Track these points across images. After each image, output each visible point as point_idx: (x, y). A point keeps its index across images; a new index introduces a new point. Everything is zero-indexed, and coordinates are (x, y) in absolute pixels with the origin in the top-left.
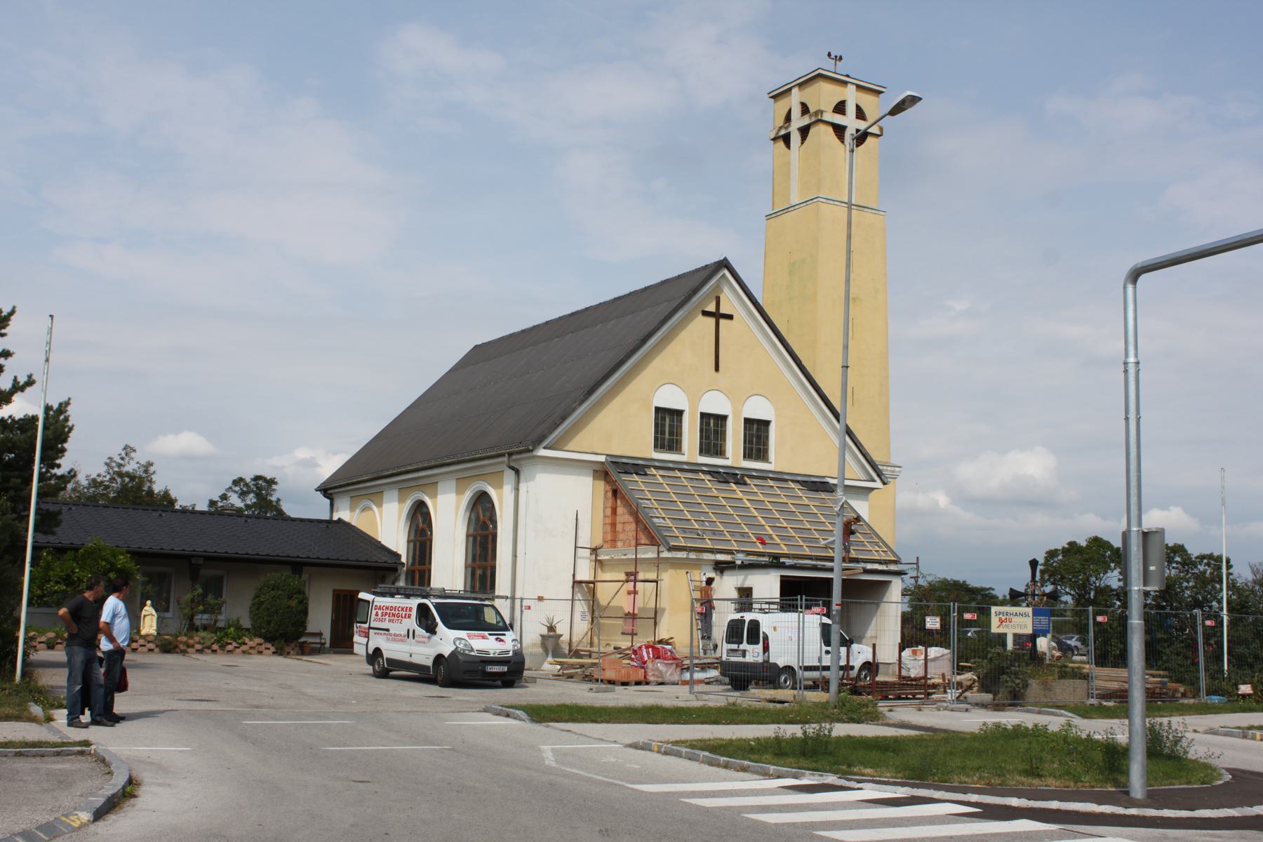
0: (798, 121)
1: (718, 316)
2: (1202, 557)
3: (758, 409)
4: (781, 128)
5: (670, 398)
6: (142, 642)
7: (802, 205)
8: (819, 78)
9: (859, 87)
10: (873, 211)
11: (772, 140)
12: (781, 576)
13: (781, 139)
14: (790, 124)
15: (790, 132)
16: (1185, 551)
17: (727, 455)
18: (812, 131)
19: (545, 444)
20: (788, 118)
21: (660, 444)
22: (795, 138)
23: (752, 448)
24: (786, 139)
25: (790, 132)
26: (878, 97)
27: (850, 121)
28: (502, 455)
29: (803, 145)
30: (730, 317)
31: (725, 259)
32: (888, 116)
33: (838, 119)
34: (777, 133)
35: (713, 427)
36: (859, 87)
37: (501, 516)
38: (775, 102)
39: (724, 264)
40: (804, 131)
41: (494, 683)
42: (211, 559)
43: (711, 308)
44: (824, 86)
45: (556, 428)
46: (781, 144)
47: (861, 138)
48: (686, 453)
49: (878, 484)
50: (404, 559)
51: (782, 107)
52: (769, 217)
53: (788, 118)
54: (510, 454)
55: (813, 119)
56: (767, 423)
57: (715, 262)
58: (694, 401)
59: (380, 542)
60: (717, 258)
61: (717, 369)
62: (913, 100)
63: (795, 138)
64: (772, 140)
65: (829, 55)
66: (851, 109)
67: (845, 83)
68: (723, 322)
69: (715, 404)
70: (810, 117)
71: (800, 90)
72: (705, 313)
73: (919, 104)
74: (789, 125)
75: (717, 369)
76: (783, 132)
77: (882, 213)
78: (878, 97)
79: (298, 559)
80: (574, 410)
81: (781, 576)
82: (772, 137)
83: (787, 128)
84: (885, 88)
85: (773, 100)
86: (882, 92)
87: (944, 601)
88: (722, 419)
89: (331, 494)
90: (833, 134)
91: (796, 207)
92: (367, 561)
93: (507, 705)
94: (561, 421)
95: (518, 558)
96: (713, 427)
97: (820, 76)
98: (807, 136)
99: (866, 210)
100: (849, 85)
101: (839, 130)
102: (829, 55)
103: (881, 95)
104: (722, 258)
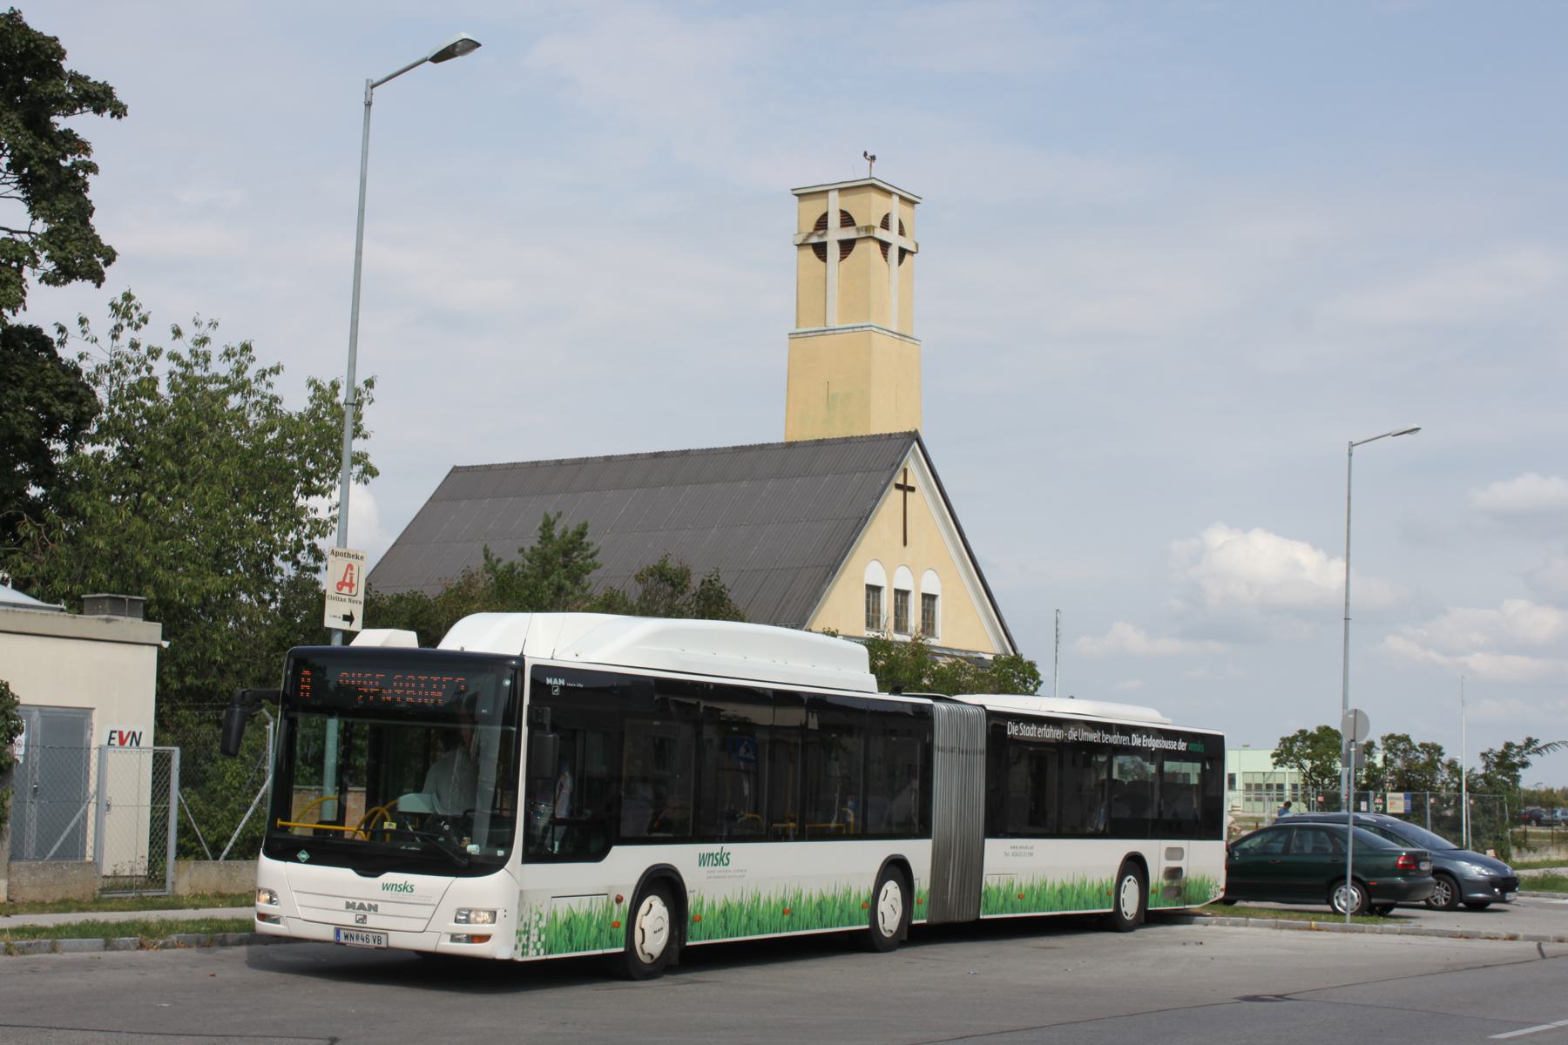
0: (835, 234)
1: (906, 488)
2: (1422, 745)
5: (875, 576)
8: (870, 188)
9: (902, 198)
11: (797, 245)
13: (811, 247)
14: (825, 232)
16: (1409, 740)
18: (858, 247)
20: (822, 223)
22: (833, 251)
26: (913, 208)
27: (891, 236)
31: (916, 431)
32: (428, 62)
34: (805, 240)
35: (902, 595)
36: (902, 198)
38: (800, 201)
39: (914, 437)
40: (847, 246)
41: (1417, 903)
43: (900, 481)
44: (876, 197)
46: (810, 252)
47: (903, 252)
51: (814, 210)
52: (793, 336)
55: (863, 234)
60: (907, 427)
61: (905, 544)
62: (470, 45)
63: (833, 251)
64: (797, 245)
65: (865, 154)
67: (890, 193)
68: (909, 494)
69: (903, 581)
70: (858, 229)
71: (840, 196)
73: (477, 50)
74: (825, 234)
75: (905, 544)
76: (815, 240)
77: (917, 342)
78: (913, 208)
82: (798, 243)
84: (920, 198)
85: (797, 198)
86: (917, 203)
91: (836, 332)
93: (1402, 920)
94: (634, 592)
97: (873, 186)
98: (851, 250)
101: (885, 246)
102: (865, 154)
103: (916, 205)
104: (913, 430)
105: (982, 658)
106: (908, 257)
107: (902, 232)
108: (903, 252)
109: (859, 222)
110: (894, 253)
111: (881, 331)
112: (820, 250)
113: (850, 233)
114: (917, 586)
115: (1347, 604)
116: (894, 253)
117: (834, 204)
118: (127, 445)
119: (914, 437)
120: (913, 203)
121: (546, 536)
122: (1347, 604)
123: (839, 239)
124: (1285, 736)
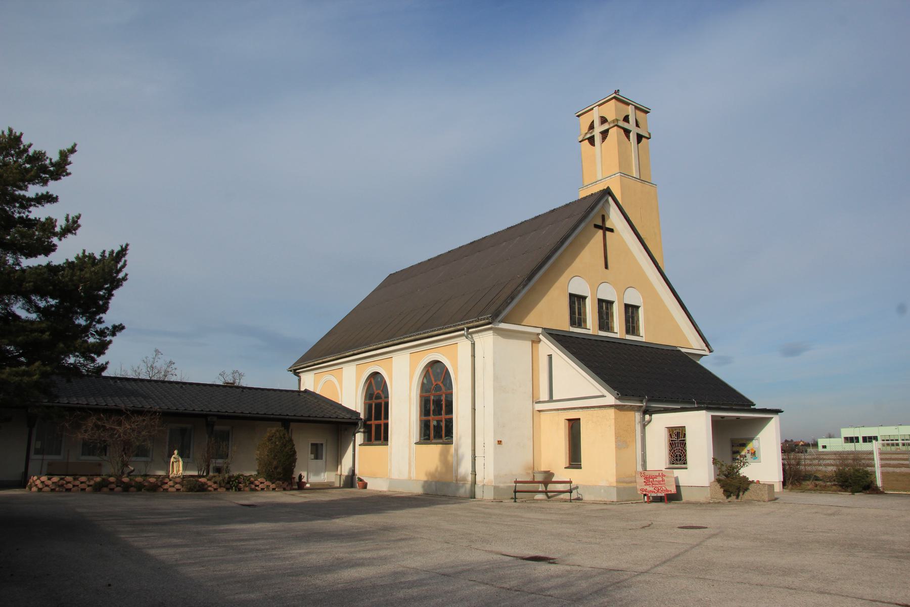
0: (598, 129)
3: (633, 297)
4: (586, 133)
5: (578, 286)
6: (171, 483)
7: (607, 179)
10: (650, 184)
12: (712, 416)
15: (594, 135)
17: (615, 331)
19: (500, 318)
20: (592, 127)
21: (573, 323)
22: (598, 139)
23: (630, 325)
24: (591, 140)
25: (594, 135)
27: (631, 126)
28: (463, 329)
29: (606, 140)
30: (611, 230)
31: (608, 188)
33: (626, 125)
35: (604, 306)
36: (636, 108)
37: (456, 379)
39: (607, 192)
40: (605, 134)
42: (222, 417)
43: (600, 223)
45: (507, 306)
47: (640, 138)
48: (591, 329)
49: (707, 353)
50: (362, 416)
53: (592, 127)
54: (468, 328)
55: (612, 125)
56: (637, 307)
57: (601, 191)
58: (594, 290)
59: (341, 404)
61: (606, 267)
63: (598, 139)
66: (632, 120)
67: (628, 104)
68: (608, 233)
69: (607, 292)
70: (609, 123)
72: (596, 226)
75: (606, 267)
76: (588, 136)
77: (655, 186)
79: (288, 417)
80: (519, 292)
81: (712, 416)
83: (591, 133)
87: (102, 425)
88: (611, 303)
89: (299, 373)
90: (624, 135)
92: (302, 416)
95: (476, 411)
96: (604, 306)
99: (646, 183)
100: (630, 105)
101: (627, 132)
104: (605, 188)
105: (679, 351)
106: (644, 140)
107: (637, 125)
108: (640, 138)
109: (609, 119)
110: (633, 136)
111: (627, 176)
112: (591, 140)
113: (606, 126)
114: (620, 299)
115: (534, 466)
116: (633, 136)
117: (595, 115)
118: (35, 237)
119: (607, 192)
120: (647, 112)
121: (67, 220)
122: (534, 466)
123: (600, 131)
124: (79, 229)
